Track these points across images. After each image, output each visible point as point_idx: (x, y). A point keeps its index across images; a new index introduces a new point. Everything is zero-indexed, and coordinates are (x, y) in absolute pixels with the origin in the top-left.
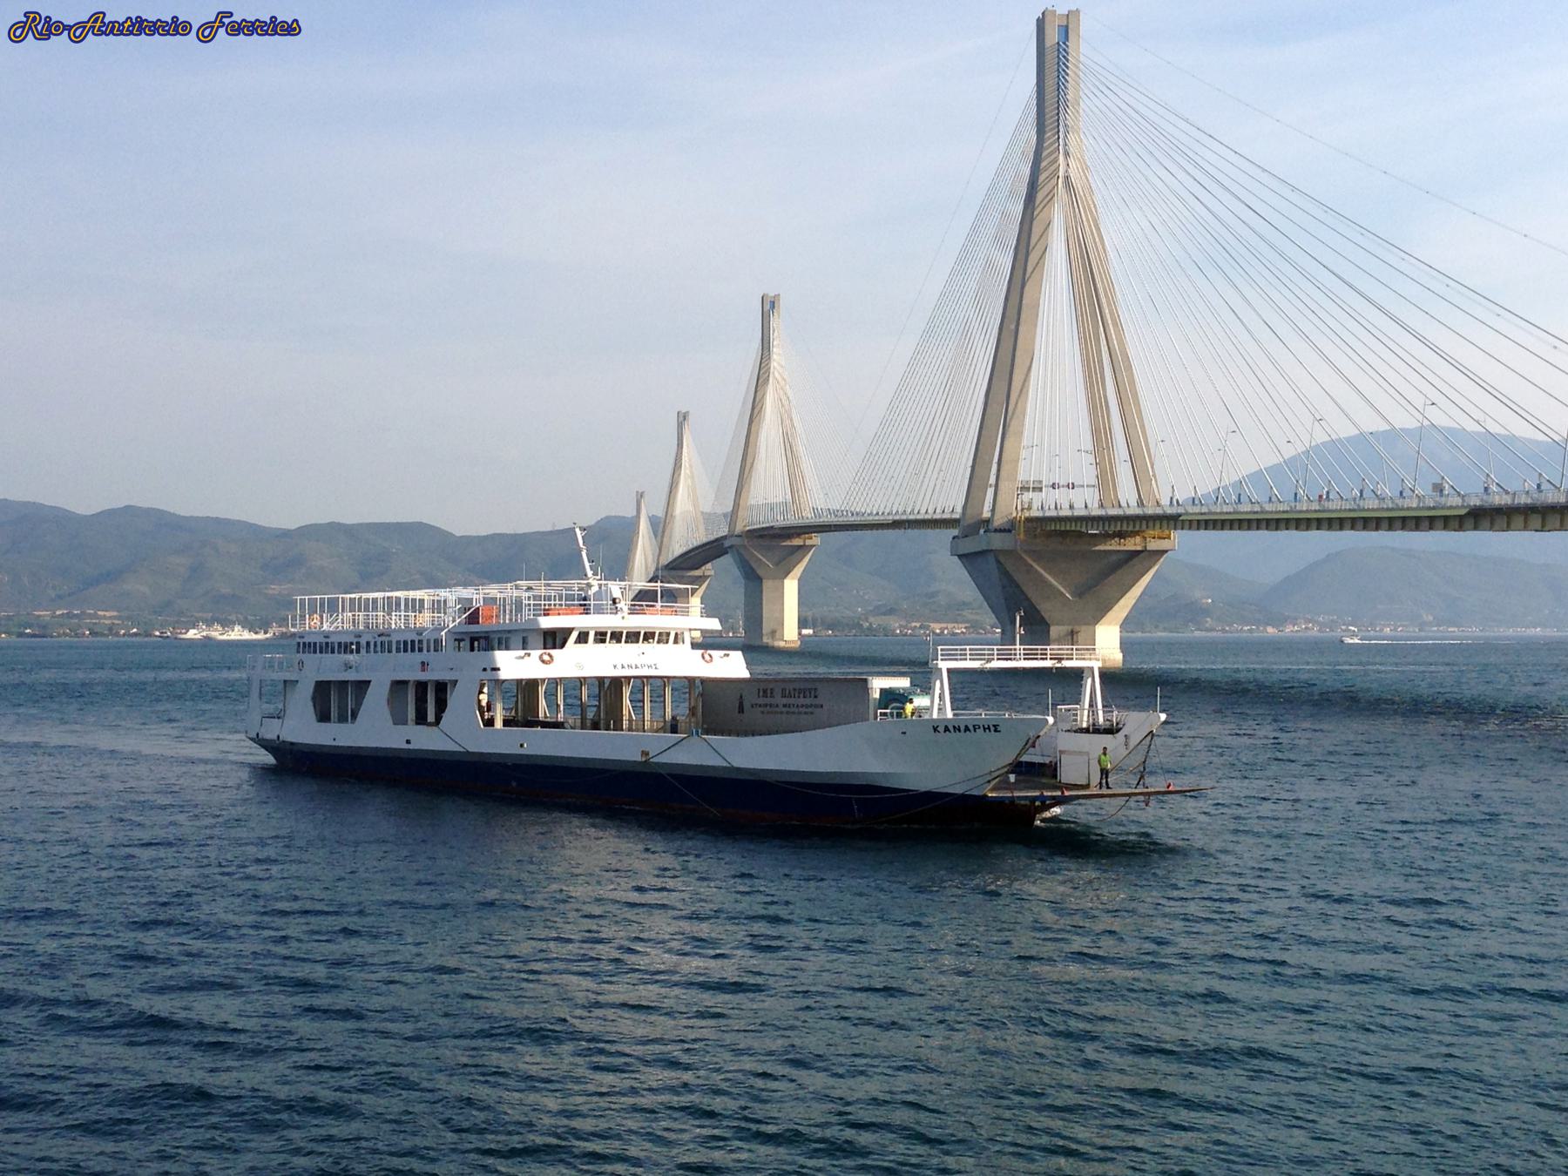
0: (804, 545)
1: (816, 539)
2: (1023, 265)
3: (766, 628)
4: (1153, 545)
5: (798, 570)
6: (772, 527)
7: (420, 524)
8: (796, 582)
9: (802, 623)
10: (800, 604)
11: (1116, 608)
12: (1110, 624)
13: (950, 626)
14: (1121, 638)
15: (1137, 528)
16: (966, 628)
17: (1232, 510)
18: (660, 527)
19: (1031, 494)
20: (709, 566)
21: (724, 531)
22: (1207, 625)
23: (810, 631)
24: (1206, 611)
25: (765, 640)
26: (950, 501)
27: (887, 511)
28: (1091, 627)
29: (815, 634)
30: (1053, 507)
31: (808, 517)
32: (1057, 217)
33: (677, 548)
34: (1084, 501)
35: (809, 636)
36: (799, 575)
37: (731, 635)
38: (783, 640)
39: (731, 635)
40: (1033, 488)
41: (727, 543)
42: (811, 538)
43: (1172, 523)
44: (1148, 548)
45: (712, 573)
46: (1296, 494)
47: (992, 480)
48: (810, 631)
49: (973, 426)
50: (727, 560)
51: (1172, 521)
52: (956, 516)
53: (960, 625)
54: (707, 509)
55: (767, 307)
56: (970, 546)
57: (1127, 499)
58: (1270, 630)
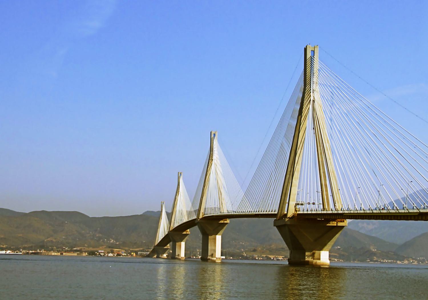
0: (224, 223)
1: (228, 221)
3: (210, 253)
4: (340, 224)
5: (222, 232)
7: (43, 211)
8: (220, 236)
10: (222, 247)
11: (220, 232)
13: (276, 256)
14: (221, 250)
15: (336, 218)
16: (283, 258)
17: (395, 212)
18: (170, 216)
19: (300, 206)
20: (188, 230)
21: (195, 217)
22: (375, 260)
24: (374, 254)
25: (209, 257)
26: (274, 209)
27: (242, 211)
29: (226, 259)
30: (315, 210)
31: (225, 212)
32: (308, 123)
33: (176, 224)
34: (316, 209)
35: (224, 259)
36: (222, 234)
37: (194, 257)
38: (215, 257)
39: (194, 257)
40: (301, 204)
41: (196, 222)
42: (226, 220)
43: (342, 216)
44: (338, 225)
45: (189, 233)
46: (361, 208)
47: (287, 201)
49: (282, 184)
50: (196, 228)
51: (343, 216)
52: (276, 213)
53: (281, 257)
54: (189, 210)
55: (179, 175)
56: (280, 223)
57: (330, 209)
58: (398, 262)
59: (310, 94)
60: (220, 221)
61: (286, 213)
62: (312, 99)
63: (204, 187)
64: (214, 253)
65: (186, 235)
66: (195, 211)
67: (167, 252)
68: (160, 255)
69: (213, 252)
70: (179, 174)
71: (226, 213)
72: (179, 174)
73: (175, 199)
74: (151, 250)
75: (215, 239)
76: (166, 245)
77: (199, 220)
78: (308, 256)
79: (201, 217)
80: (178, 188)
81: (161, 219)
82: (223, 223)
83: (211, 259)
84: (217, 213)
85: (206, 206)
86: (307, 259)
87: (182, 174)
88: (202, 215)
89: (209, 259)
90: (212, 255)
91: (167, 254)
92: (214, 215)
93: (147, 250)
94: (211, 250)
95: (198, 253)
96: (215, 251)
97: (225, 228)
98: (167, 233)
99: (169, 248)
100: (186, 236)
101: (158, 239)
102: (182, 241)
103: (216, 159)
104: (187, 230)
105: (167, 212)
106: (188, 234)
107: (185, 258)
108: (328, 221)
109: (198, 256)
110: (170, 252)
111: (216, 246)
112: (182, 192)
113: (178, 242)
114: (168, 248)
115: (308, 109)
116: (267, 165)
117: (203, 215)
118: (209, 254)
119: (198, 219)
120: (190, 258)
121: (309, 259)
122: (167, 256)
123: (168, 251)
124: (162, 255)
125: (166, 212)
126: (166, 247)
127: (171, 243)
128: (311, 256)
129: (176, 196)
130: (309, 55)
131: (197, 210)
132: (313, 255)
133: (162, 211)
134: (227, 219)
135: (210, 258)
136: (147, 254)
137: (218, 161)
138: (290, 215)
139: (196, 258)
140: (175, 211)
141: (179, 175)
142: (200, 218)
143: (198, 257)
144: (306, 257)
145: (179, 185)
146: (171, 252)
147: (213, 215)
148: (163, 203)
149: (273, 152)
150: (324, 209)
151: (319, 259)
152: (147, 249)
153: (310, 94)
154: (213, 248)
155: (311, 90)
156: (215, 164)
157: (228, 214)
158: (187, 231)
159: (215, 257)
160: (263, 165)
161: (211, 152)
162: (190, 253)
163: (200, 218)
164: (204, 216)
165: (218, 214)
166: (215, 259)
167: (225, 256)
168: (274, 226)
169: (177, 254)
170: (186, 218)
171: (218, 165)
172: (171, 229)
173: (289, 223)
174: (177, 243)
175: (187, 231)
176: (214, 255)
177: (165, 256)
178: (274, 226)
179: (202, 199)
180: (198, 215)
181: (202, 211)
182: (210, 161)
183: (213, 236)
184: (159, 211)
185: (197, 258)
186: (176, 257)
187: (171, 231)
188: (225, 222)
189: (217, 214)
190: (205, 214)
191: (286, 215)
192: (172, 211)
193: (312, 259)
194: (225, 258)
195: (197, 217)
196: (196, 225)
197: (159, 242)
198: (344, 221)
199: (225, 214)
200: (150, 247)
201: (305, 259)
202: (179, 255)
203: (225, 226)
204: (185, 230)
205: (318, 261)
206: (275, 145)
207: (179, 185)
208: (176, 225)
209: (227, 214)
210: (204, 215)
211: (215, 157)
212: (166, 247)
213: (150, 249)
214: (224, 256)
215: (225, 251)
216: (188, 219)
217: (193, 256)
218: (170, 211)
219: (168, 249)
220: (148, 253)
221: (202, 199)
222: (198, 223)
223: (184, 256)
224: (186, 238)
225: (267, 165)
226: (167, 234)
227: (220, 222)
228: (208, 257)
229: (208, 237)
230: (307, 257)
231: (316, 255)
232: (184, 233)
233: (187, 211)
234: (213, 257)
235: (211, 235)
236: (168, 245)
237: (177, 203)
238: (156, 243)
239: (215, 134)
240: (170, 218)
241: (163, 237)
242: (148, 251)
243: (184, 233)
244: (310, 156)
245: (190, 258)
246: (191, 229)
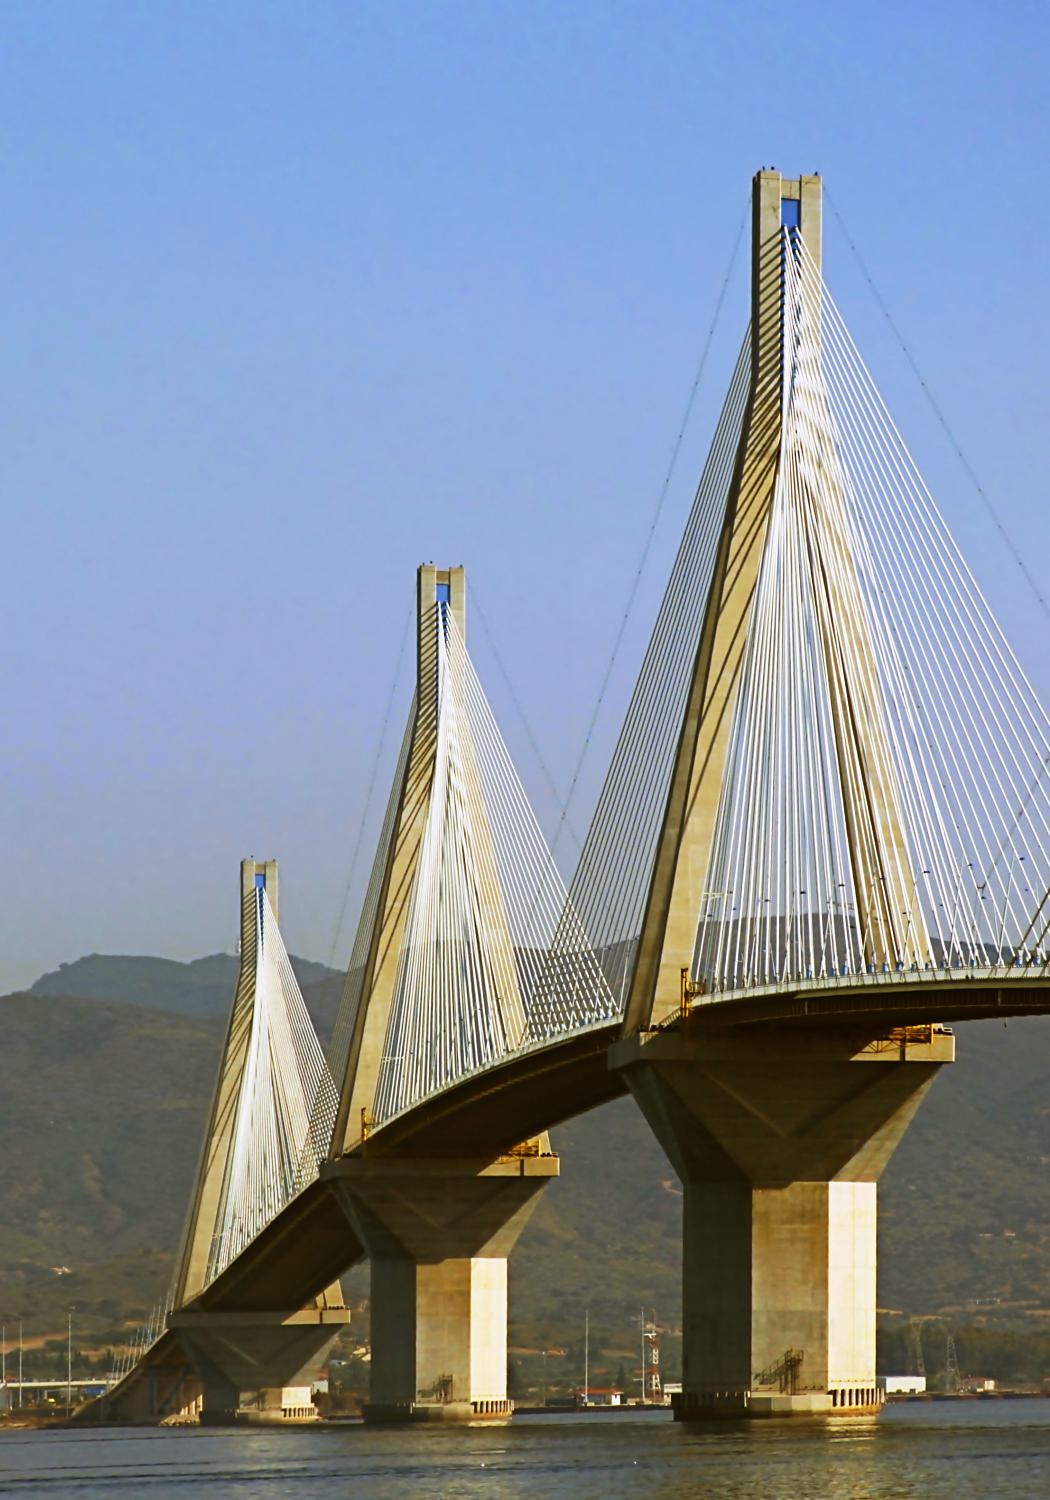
1: (942, 1045)
2: (703, 681)
3: (763, 1354)
5: (880, 1149)
6: (788, 997)
8: (870, 1189)
9: (890, 1359)
12: (493, 1255)
14: (880, 1319)
20: (542, 1141)
23: (918, 1384)
25: (757, 1392)
28: (463, 1260)
29: (933, 1394)
35: (912, 1398)
37: (616, 1401)
38: (821, 1388)
39: (616, 1401)
41: (618, 1057)
42: (928, 1040)
45: (555, 1167)
48: (918, 1384)
54: (542, 941)
55: (431, 595)
59: (774, 418)
60: (868, 1042)
63: (693, 723)
64: (811, 1349)
66: (609, 956)
67: (319, 1358)
68: (244, 1396)
69: (792, 1341)
70: (430, 582)
71: (914, 968)
72: (430, 582)
73: (395, 835)
74: (146, 1349)
76: (304, 1297)
77: (644, 1038)
78: (249, 1403)
79: (666, 1008)
80: (415, 729)
81: (237, 1036)
83: (775, 1407)
84: (831, 972)
85: (717, 903)
87: (460, 595)
88: (677, 992)
89: (757, 1408)
90: (789, 1372)
91: (323, 1387)
92: (804, 986)
93: (94, 1356)
94: (782, 1320)
95: (655, 1360)
96: (816, 1326)
97: (911, 1110)
98: (310, 1175)
99: (346, 1317)
100: (524, 1199)
101: (216, 1244)
102: (473, 1252)
103: (810, 443)
104: (530, 1142)
105: (304, 963)
106: (539, 1181)
107: (512, 1406)
109: (656, 1380)
110: (356, 1363)
111: (823, 1282)
112: (458, 763)
113: (435, 1259)
114: (331, 1318)
116: (645, 796)
117: (688, 995)
118: (762, 1358)
119: (643, 1025)
120: (573, 1405)
121: (429, 1402)
122: (316, 1398)
123: (334, 1355)
124: (260, 1399)
125: (291, 957)
126: (303, 1317)
127: (363, 1271)
129: (401, 808)
131: (615, 949)
133: (248, 959)
134: (935, 1026)
135: (775, 1395)
136: (102, 1387)
137: (834, 467)
139: (631, 1402)
140: (397, 949)
141: (431, 595)
142: (654, 1022)
143: (649, 1395)
145: (436, 701)
146: (368, 1358)
147: (793, 987)
148: (262, 878)
152: (96, 1341)
153: (774, 418)
154: (800, 1302)
155: (780, 397)
156: (801, 487)
157: (941, 976)
158: (531, 1153)
159: (466, 1400)
160: (648, 784)
161: (755, 381)
162: (575, 1356)
163: (654, 1022)
164: (696, 1002)
165: (844, 982)
166: (819, 1402)
167: (929, 1375)
169: (424, 1377)
170: (515, 1016)
171: (828, 502)
172: (353, 1137)
175: (531, 1153)
176: (804, 1370)
177: (297, 1398)
179: (672, 832)
180: (644, 984)
181: (679, 951)
182: (753, 467)
183: (796, 1192)
184: (223, 957)
185: (640, 1407)
186: (419, 1404)
187: (354, 1155)
188: (915, 1053)
189: (832, 983)
190: (704, 988)
192: (362, 961)
193: (438, 1401)
194: (929, 1387)
195: (626, 1012)
196: (620, 1090)
197: (223, 1266)
199: (912, 978)
200: (130, 1324)
202: (445, 1386)
203: (914, 1088)
204: (508, 1137)
207: (426, 695)
208: (411, 1095)
209: (927, 977)
210: (703, 992)
211: (801, 426)
212: (303, 1317)
213: (135, 1337)
214: (917, 1374)
215: (927, 1328)
216: (534, 1028)
217: (602, 1387)
218: (341, 961)
219: (334, 1328)
220: (113, 1381)
221: (672, 832)
222: (636, 1067)
223: (499, 1392)
224: (524, 1215)
225: (645, 796)
226: (315, 1188)
228: (413, 1399)
230: (761, 1383)
232: (502, 1168)
233: (518, 953)
234: (447, 1402)
235: (781, 1182)
236: (333, 1293)
237: (412, 875)
238: (201, 1276)
239: (793, 208)
240: (344, 1026)
241: (271, 1215)
242: (106, 1366)
243: (502, 1168)
244: (815, 777)
245: (573, 1405)
246: (562, 1127)
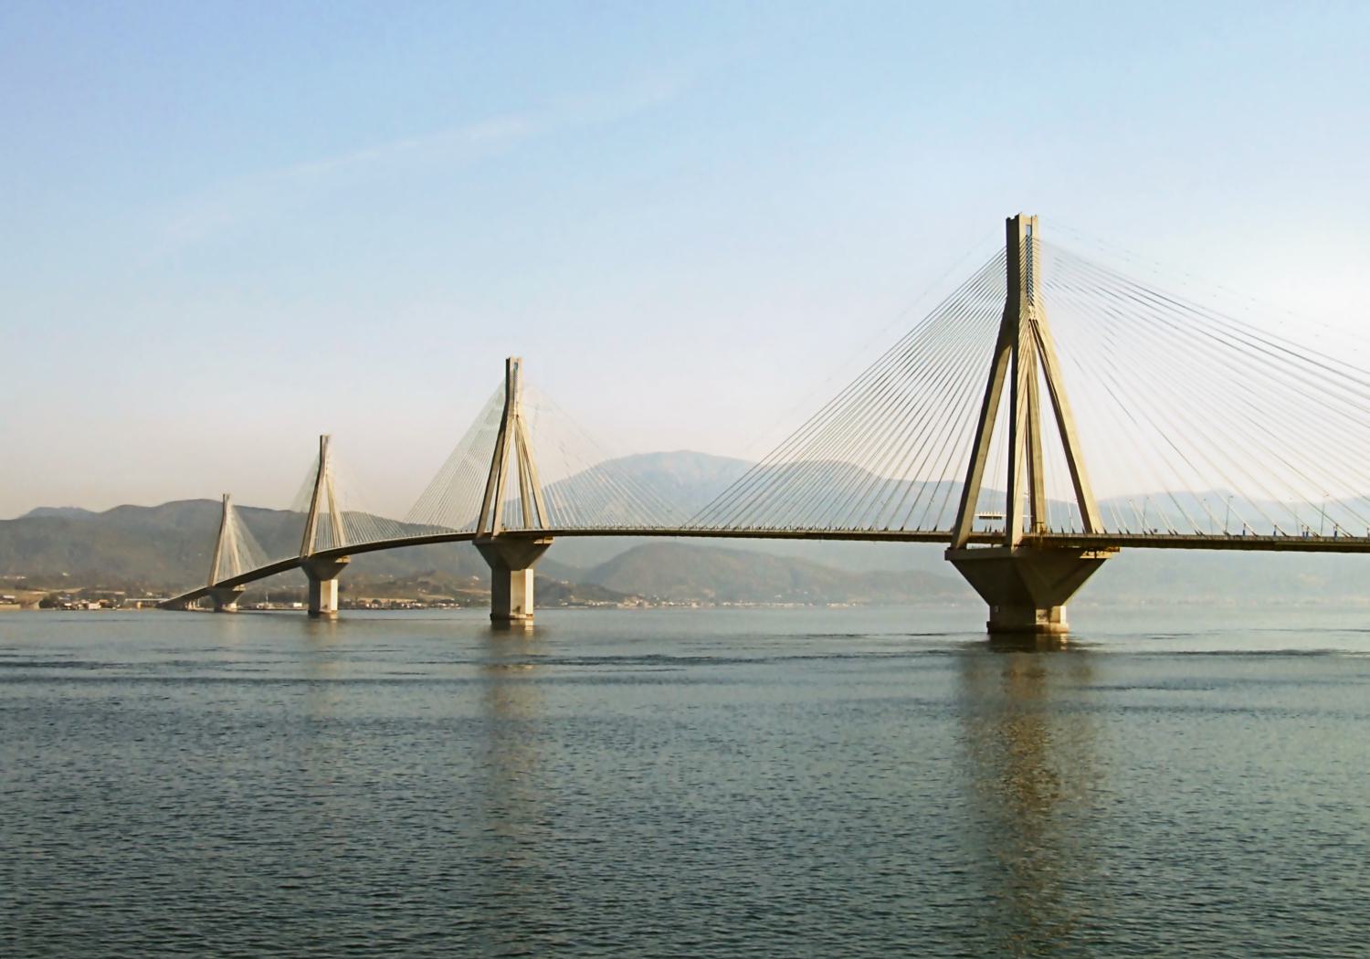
4: (546, 542)
25: (512, 614)
52: (475, 532)
57: (533, 526)
61: (490, 531)
62: (515, 413)
65: (343, 565)
75: (523, 578)
78: (1041, 617)
82: (1092, 559)
86: (1039, 622)
96: (523, 600)
108: (536, 539)
115: (511, 426)
128: (1044, 616)
130: (512, 368)
132: (1048, 615)
138: (496, 533)
144: (1037, 619)
149: (845, 400)
150: (525, 527)
151: (1059, 621)
166: (521, 616)
168: (946, 559)
169: (322, 604)
173: (1016, 555)
174: (323, 583)
178: (946, 559)
191: (490, 535)
198: (1119, 550)
201: (1035, 621)
205: (1058, 625)
206: (922, 367)
227: (1082, 557)
229: (510, 574)
231: (1054, 614)
